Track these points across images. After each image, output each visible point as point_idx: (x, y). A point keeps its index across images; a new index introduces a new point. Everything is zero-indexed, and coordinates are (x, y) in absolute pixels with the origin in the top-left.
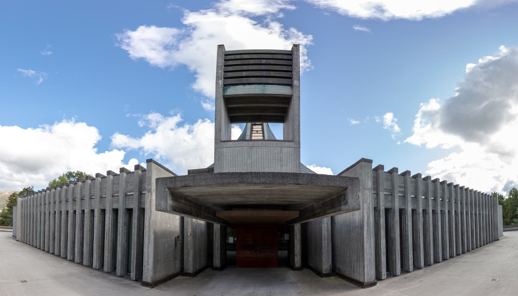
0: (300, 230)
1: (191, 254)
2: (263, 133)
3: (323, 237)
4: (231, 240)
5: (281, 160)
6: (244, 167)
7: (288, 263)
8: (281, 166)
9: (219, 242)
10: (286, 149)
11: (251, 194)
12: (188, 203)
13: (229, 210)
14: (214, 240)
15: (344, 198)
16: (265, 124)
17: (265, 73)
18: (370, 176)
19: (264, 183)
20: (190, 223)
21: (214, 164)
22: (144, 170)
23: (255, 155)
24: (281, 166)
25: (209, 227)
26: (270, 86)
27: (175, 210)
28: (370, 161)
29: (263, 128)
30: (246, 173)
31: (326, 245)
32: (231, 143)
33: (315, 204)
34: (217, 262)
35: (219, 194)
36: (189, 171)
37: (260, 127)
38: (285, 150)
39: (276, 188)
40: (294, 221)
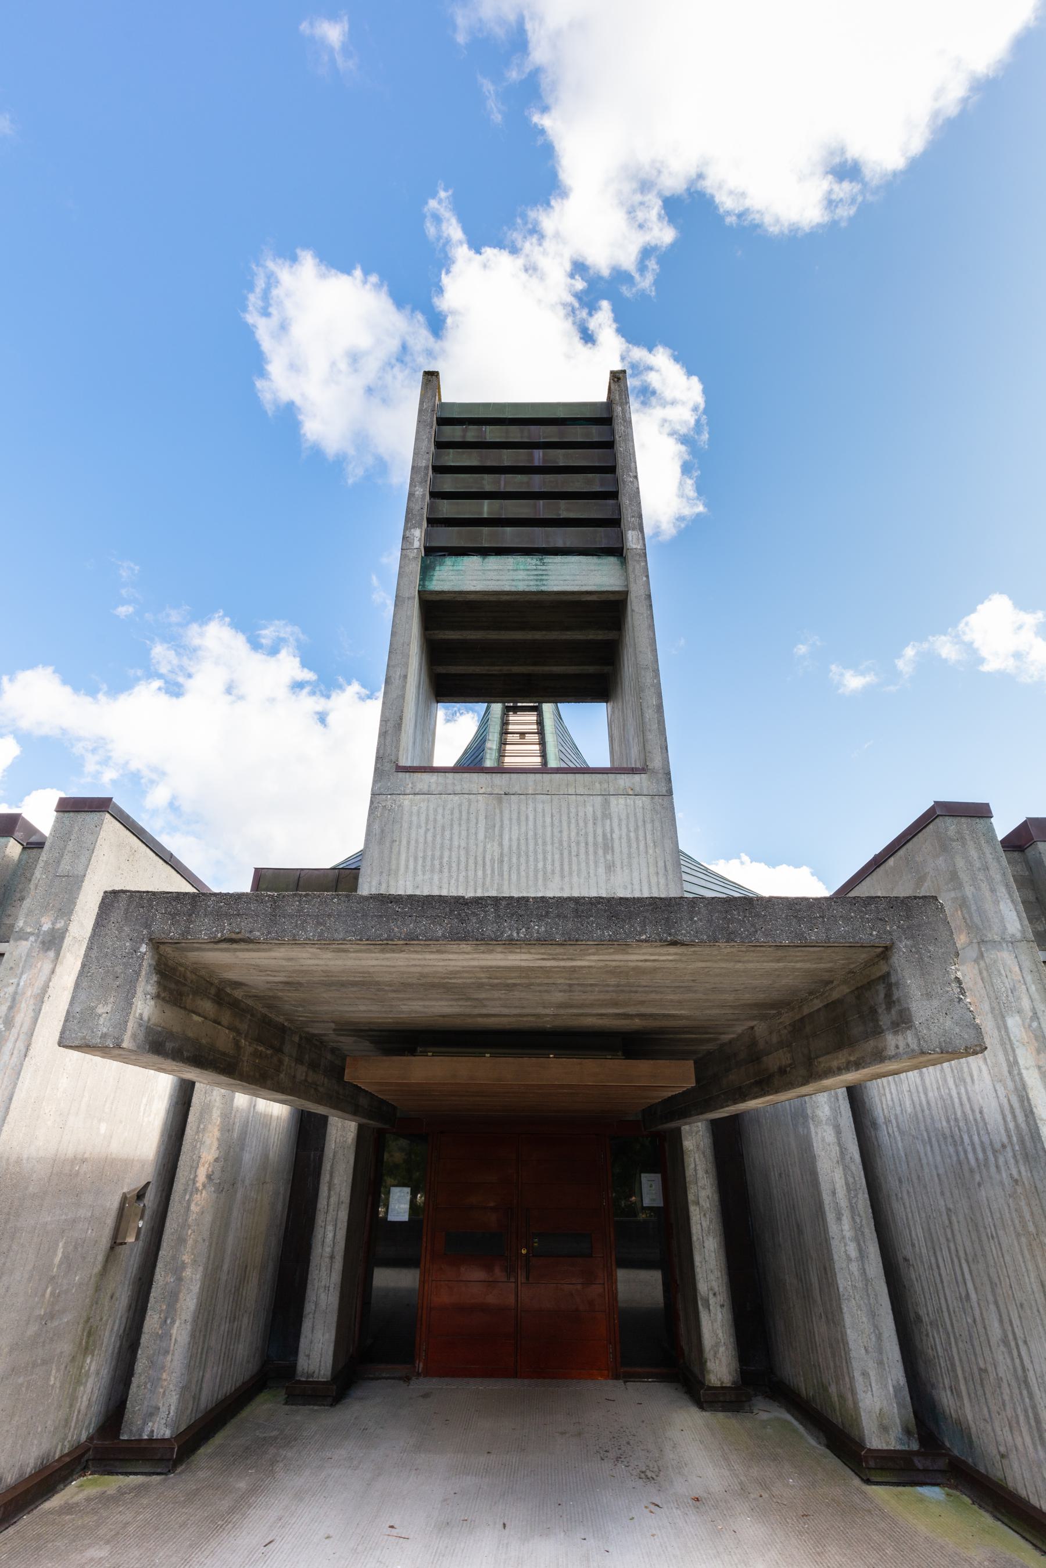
0: (709, 1152)
1: (188, 1303)
2: (542, 743)
3: (827, 1198)
4: (399, 1205)
5: (608, 847)
6: (471, 874)
7: (660, 1354)
8: (610, 868)
9: (343, 1215)
10: (622, 800)
11: (494, 987)
12: (226, 1018)
13: (401, 1052)
14: (322, 1203)
15: (888, 996)
16: (547, 708)
17: (543, 509)
18: (998, 877)
19: (543, 941)
20: (216, 1115)
21: (361, 855)
22: (34, 845)
23: (515, 828)
24: (610, 868)
25: (307, 1133)
26: (558, 559)
27: (159, 1046)
28: (980, 812)
29: (540, 723)
30: (478, 902)
31: (852, 1250)
32: (433, 778)
33: (761, 1028)
34: (318, 1348)
35: (366, 984)
36: (261, 877)
37: (532, 717)
38: (618, 805)
39: (591, 960)
40: (682, 1107)
